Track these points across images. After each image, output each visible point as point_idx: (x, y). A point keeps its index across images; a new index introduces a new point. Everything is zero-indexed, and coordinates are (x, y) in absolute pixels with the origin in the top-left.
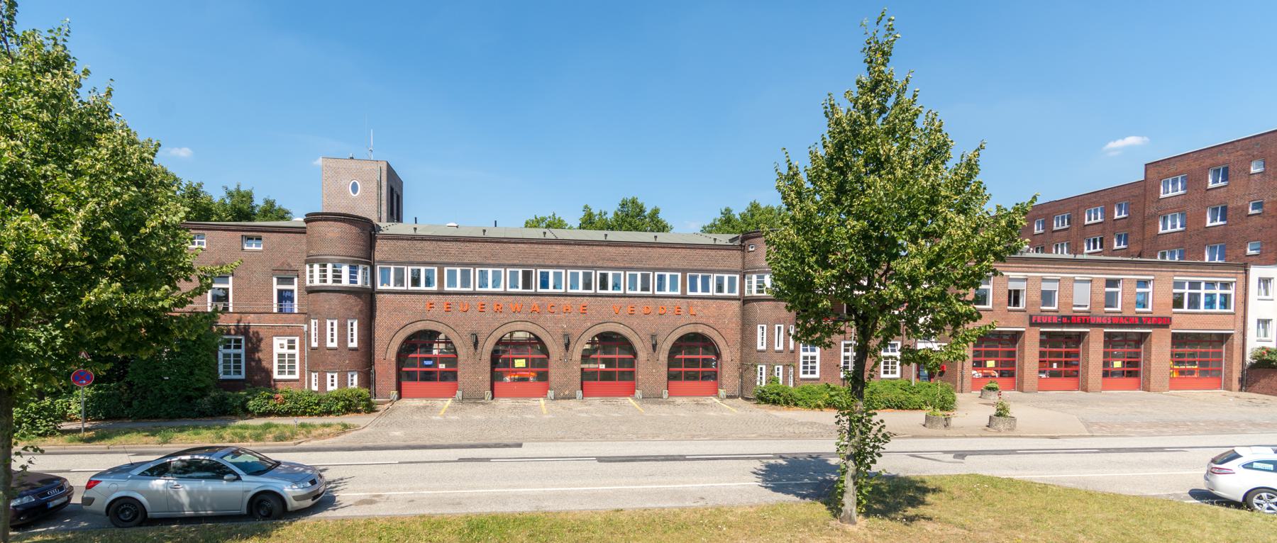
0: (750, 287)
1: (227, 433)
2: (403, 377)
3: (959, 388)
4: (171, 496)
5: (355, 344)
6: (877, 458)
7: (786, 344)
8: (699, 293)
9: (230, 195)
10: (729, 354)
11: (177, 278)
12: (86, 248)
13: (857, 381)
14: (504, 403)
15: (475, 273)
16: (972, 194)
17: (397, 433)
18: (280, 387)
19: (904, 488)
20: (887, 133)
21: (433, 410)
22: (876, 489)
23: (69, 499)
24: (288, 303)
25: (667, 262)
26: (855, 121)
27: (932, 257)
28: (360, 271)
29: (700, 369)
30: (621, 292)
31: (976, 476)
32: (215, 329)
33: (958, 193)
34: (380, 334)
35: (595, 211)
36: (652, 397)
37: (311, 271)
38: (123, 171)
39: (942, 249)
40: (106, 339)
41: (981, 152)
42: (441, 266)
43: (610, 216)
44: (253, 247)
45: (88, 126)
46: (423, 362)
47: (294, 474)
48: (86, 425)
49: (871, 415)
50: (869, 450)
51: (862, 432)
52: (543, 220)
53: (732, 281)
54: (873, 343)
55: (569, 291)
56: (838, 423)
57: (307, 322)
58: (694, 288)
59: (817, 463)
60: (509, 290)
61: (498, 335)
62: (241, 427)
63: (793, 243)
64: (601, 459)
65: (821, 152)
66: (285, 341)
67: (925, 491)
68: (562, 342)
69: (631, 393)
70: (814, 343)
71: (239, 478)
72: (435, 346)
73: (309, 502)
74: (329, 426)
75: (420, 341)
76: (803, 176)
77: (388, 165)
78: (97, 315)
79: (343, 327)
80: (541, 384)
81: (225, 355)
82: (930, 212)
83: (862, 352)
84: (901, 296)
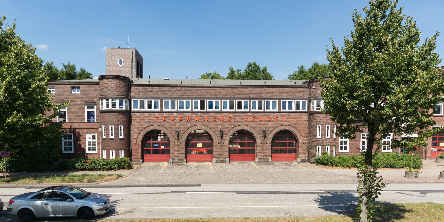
0: (313, 107)
1: (67, 179)
2: (144, 152)
3: (424, 157)
4: (45, 208)
5: (122, 137)
6: (378, 195)
7: (332, 136)
8: (287, 110)
9: (65, 67)
10: (302, 140)
11: (45, 109)
12: (7, 98)
13: (368, 157)
14: (192, 164)
16: (431, 60)
17: (142, 179)
18: (89, 157)
19: (393, 210)
20: (385, 29)
21: (159, 168)
22: (378, 210)
23: (2, 208)
24: (92, 117)
25: (271, 95)
26: (369, 24)
27: (408, 93)
28: (124, 102)
29: (288, 148)
30: (248, 110)
31: (431, 203)
32: (60, 130)
33: (423, 60)
35: (235, 69)
36: (263, 161)
37: (102, 103)
38: (21, 63)
39: (414, 90)
40: (16, 139)
41: (437, 37)
42: (161, 99)
43: (243, 72)
44: (76, 92)
45: (6, 42)
46: (153, 145)
47: (97, 199)
48: (7, 174)
49: (376, 173)
50: (374, 191)
51: (370, 182)
52: (210, 74)
53: (304, 104)
54: (378, 136)
55: (223, 110)
56: (358, 177)
57: (101, 126)
58: (284, 108)
59: (347, 196)
61: (188, 132)
62: (73, 176)
63: (336, 88)
64: (238, 193)
65: (350, 40)
66: (91, 135)
67: (404, 211)
68: (219, 135)
69: (253, 160)
70: (346, 137)
71: (73, 201)
72: (159, 137)
73: (104, 212)
74: (111, 175)
75: (152, 135)
76: (341, 52)
77: (136, 51)
78: (12, 128)
80: (209, 155)
81: (65, 142)
82: (408, 70)
83: (371, 141)
84: (391, 114)
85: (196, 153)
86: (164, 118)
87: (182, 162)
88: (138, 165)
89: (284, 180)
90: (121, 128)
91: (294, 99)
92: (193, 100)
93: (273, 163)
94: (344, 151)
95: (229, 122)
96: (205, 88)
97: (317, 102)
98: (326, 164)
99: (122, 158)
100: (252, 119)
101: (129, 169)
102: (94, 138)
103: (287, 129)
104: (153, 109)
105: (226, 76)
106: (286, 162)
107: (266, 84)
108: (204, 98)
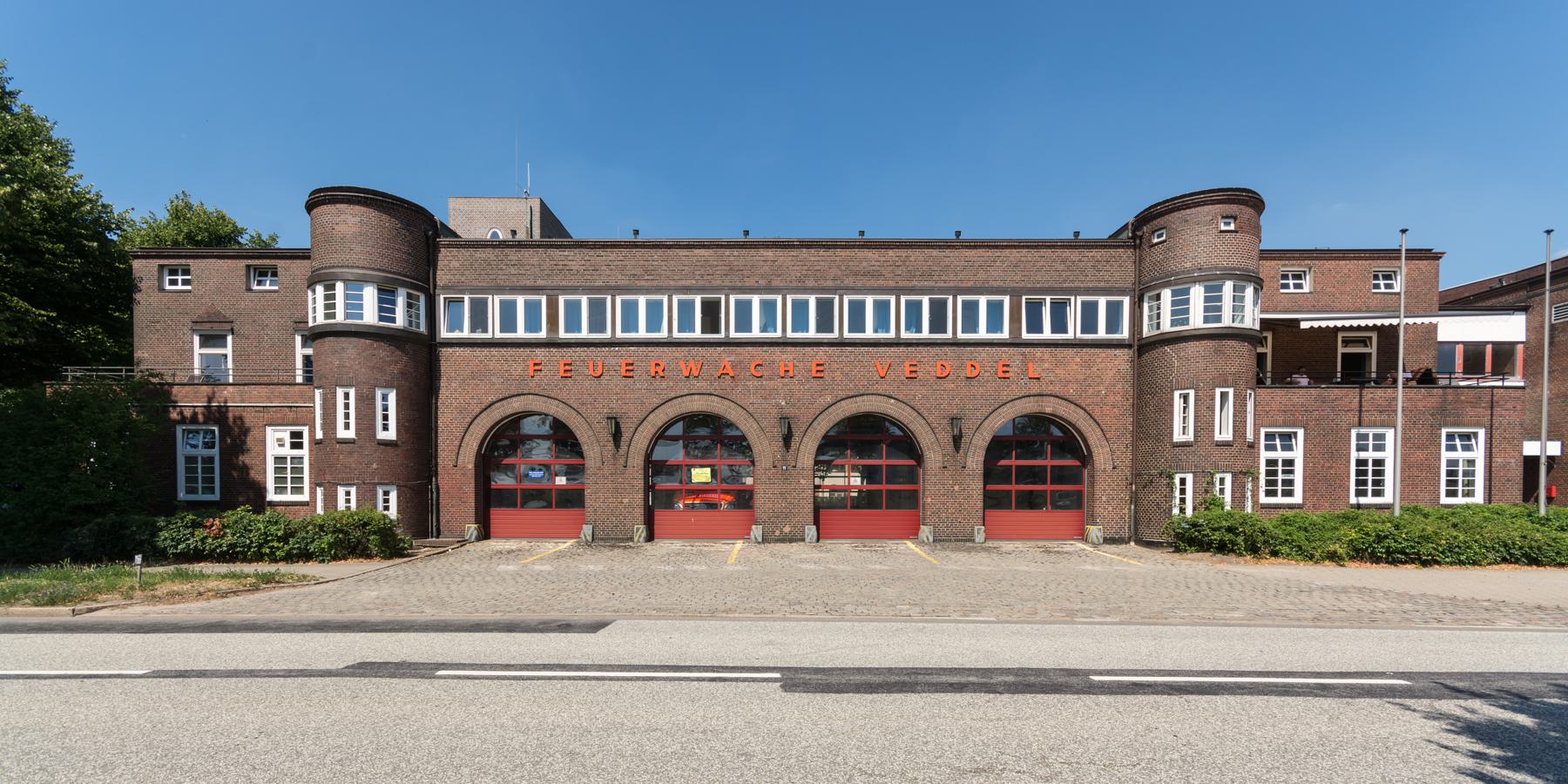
2: (488, 502)
5: (391, 434)
8: (1047, 334)
10: (1108, 458)
14: (663, 546)
15: (615, 305)
25: (982, 275)
28: (401, 301)
36: (953, 538)
46: (524, 476)
58: (1035, 326)
60: (676, 334)
64: (797, 680)
68: (778, 432)
69: (912, 533)
79: (366, 402)
80: (741, 514)
86: (562, 368)
87: (631, 539)
90: (385, 398)
91: (1076, 292)
93: (990, 544)
94: (1279, 500)
95: (815, 383)
96: (720, 251)
97: (1174, 294)
98: (1223, 548)
101: (391, 557)
102: (297, 445)
103: (1048, 410)
108: (718, 289)
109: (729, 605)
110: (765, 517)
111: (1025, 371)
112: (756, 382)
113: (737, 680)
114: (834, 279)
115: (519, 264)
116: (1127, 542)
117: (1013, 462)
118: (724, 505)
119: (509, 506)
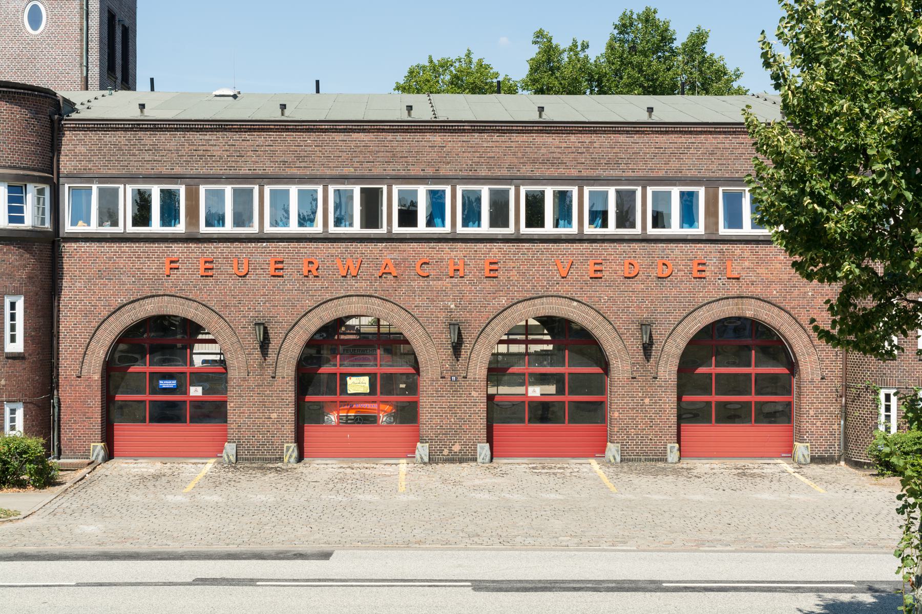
5: (18, 347)
14: (321, 468)
15: (262, 197)
25: (674, 164)
34: (71, 324)
35: (562, 42)
43: (596, 52)
52: (445, 65)
58: (734, 220)
64: (479, 586)
69: (598, 450)
75: (161, 337)
80: (404, 430)
85: (347, 421)
86: (202, 266)
87: (281, 459)
88: (85, 471)
89: (707, 536)
90: (13, 306)
92: (331, 189)
93: (686, 463)
95: (488, 285)
96: (382, 136)
99: (14, 439)
100: (592, 268)
103: (749, 314)
104: (156, 226)
105: (519, 72)
106: (741, 463)
107: (656, 117)
109: (418, 538)
110: (432, 435)
111: (722, 271)
112: (422, 283)
113: (445, 586)
114: (509, 168)
115: (155, 149)
116: (837, 462)
117: (711, 369)
118: (383, 418)
119: (135, 420)
